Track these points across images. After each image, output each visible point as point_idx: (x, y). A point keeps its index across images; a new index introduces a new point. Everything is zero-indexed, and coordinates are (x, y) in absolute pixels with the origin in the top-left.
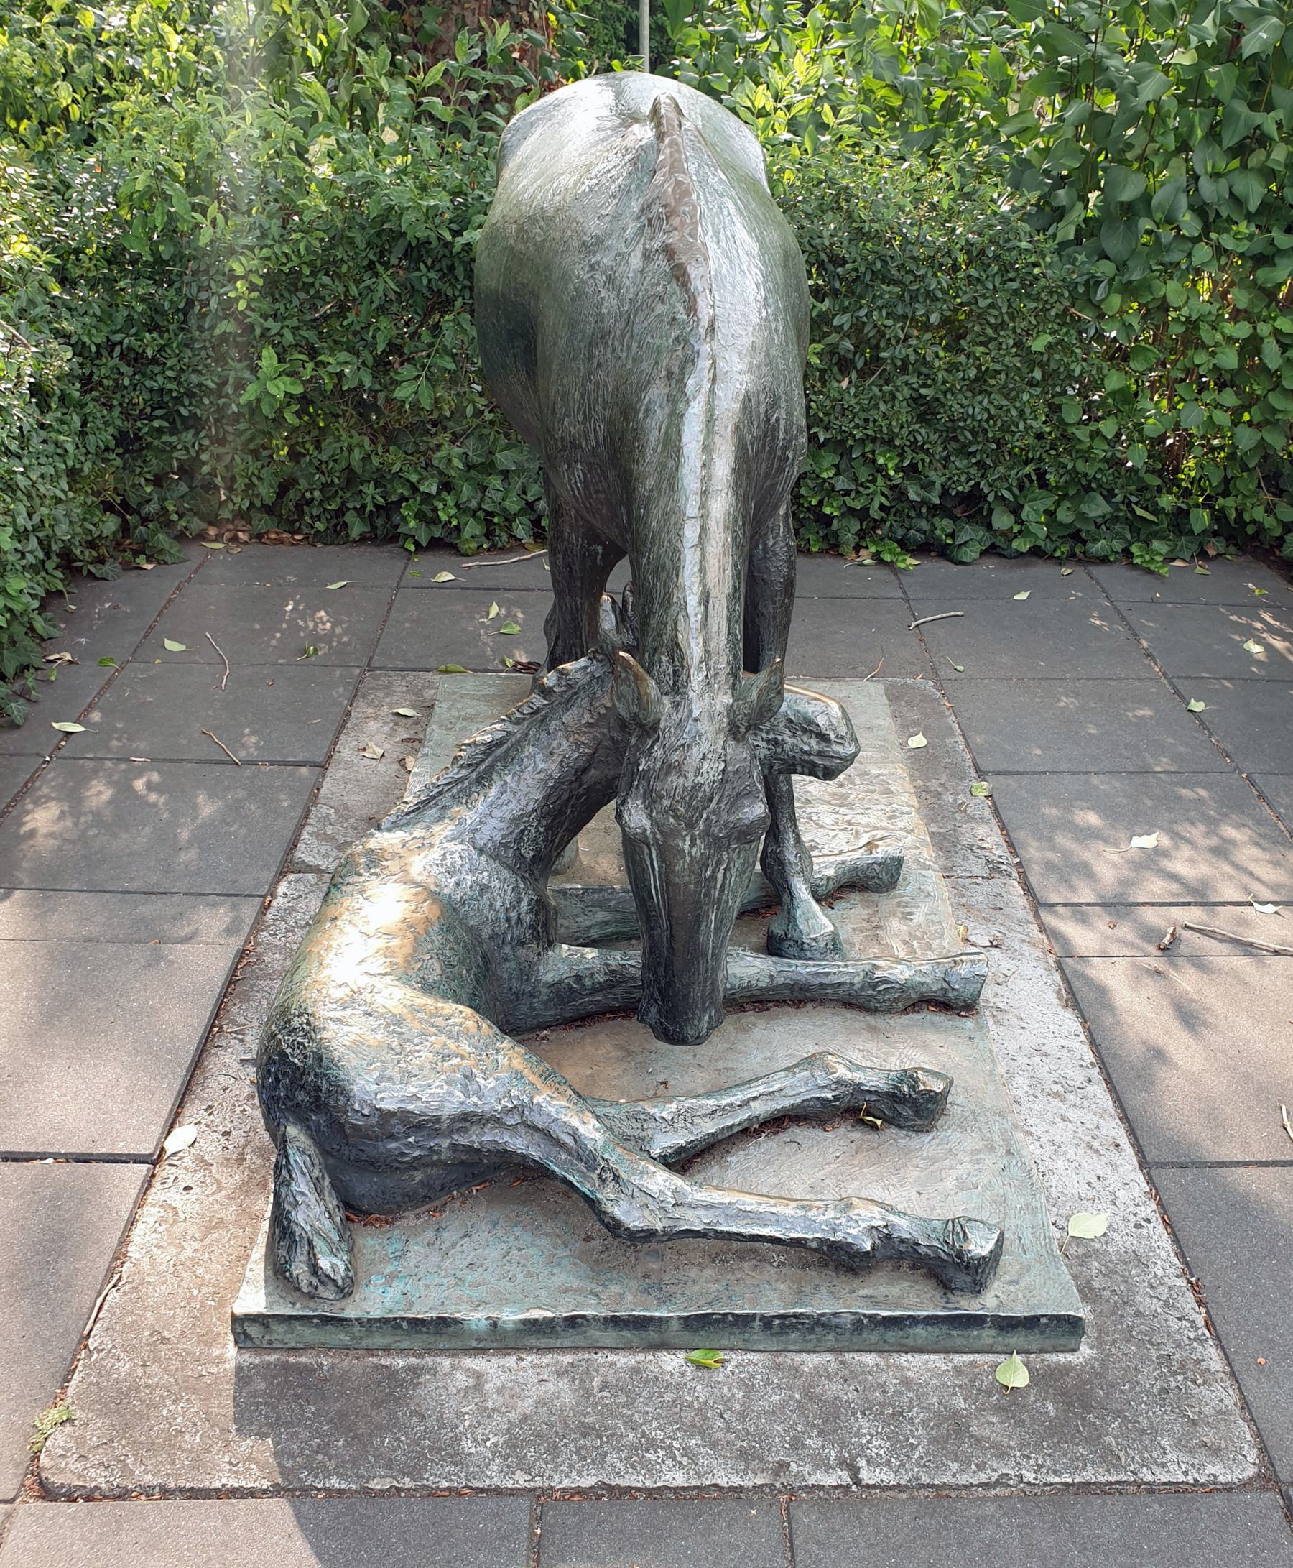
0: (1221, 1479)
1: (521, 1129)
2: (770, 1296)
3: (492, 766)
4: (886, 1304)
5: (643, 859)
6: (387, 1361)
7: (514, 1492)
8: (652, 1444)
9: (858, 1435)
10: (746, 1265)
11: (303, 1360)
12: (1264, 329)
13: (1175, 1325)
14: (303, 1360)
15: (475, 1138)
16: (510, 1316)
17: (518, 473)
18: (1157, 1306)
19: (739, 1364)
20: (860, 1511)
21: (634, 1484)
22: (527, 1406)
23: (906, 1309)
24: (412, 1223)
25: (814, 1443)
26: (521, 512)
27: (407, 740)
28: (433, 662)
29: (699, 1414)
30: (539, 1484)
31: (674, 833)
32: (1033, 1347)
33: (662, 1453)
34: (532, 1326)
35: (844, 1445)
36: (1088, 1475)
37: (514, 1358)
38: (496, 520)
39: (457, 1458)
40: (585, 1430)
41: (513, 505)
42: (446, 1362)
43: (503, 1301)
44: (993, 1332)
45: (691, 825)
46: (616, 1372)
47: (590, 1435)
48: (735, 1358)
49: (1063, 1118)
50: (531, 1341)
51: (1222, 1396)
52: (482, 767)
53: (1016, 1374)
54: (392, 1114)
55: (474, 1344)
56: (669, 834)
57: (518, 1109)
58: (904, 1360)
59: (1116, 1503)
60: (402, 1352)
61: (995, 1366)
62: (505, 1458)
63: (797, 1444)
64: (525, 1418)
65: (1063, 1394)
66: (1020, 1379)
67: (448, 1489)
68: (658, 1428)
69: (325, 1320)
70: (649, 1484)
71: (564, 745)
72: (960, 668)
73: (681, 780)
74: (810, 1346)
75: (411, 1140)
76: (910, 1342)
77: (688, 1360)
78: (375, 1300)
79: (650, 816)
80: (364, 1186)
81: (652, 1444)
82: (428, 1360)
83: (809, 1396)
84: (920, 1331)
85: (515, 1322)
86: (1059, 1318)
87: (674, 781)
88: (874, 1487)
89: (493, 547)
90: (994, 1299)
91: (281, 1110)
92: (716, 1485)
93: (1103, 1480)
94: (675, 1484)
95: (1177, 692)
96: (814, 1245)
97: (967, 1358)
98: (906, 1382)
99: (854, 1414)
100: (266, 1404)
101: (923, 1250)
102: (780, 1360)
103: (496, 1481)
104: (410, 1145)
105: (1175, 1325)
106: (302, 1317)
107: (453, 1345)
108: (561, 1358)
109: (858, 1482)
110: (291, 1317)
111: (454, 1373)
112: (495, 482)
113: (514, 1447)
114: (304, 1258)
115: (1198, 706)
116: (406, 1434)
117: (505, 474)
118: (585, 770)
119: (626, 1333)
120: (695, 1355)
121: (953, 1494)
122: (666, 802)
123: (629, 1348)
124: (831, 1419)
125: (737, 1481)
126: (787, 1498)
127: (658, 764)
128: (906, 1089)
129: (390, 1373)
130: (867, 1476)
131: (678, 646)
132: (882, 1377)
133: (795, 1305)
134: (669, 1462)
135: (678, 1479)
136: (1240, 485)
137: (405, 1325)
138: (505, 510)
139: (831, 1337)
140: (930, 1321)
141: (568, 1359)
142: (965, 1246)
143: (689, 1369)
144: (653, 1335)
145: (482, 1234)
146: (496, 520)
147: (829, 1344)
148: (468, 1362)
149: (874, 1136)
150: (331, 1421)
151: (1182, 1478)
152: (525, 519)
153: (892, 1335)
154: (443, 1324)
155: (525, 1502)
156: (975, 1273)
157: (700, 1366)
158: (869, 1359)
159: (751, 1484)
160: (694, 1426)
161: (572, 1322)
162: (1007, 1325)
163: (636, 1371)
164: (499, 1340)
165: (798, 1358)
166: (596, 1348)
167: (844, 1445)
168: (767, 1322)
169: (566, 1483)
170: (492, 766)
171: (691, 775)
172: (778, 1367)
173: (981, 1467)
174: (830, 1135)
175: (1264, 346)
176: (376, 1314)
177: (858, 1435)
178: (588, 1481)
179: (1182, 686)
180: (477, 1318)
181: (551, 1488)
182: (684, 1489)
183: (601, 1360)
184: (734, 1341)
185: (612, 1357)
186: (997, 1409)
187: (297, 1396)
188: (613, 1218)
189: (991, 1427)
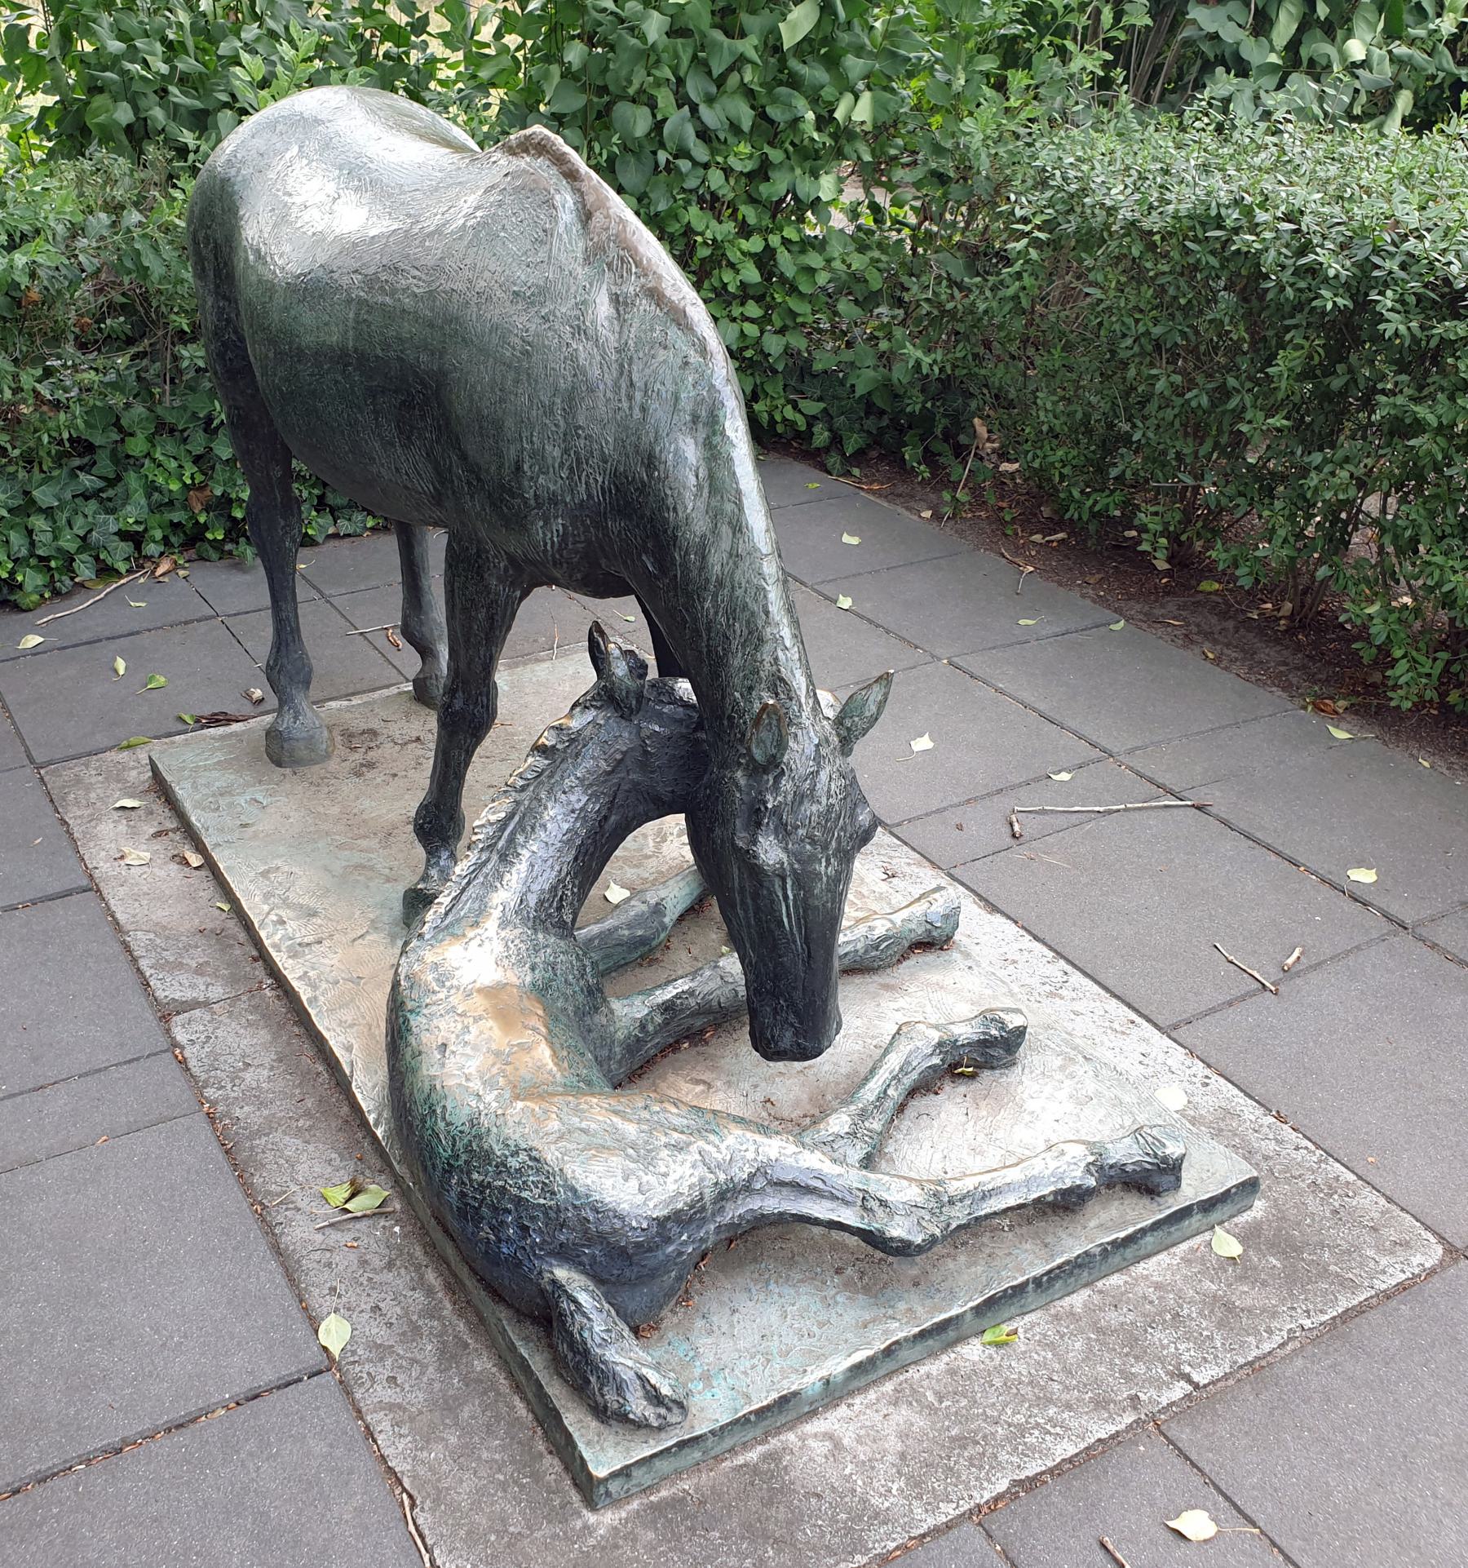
0: (1427, 1265)
1: (768, 1189)
2: (1028, 1261)
3: (511, 840)
4: (1125, 1224)
5: (772, 893)
6: (740, 1460)
7: (949, 1526)
8: (1022, 1430)
9: (1164, 1347)
10: (985, 1240)
11: (664, 1493)
12: (775, 240)
13: (1294, 1154)
14: (664, 1493)
15: (736, 1211)
16: (838, 1365)
17: (61, 508)
18: (1272, 1145)
19: (1028, 1326)
20: (1216, 1410)
21: (1039, 1470)
22: (893, 1444)
23: (1134, 1224)
24: (675, 1320)
25: (1139, 1369)
26: (80, 550)
27: (158, 834)
28: (101, 740)
29: (1039, 1386)
30: (967, 1507)
31: (813, 859)
32: (1225, 1217)
33: (1036, 1433)
34: (858, 1369)
35: (1162, 1360)
36: (1343, 1304)
37: (844, 1407)
38: (53, 564)
39: (880, 1517)
40: (961, 1442)
41: (68, 543)
42: (791, 1437)
43: (821, 1357)
44: (1199, 1216)
45: (825, 847)
46: (938, 1381)
47: (965, 1444)
48: (1019, 1323)
49: (1077, 1014)
50: (862, 1382)
51: (1369, 1202)
52: (501, 844)
53: (1227, 1244)
54: (667, 1218)
55: (806, 1409)
56: (807, 860)
57: (761, 1171)
58: (1141, 1268)
59: (1374, 1316)
60: (746, 1446)
61: (1209, 1244)
62: (919, 1497)
63: (1129, 1377)
64: (903, 1456)
65: (1273, 1245)
66: (1234, 1248)
67: (897, 1548)
68: (1014, 1414)
69: (682, 1445)
70: (1050, 1464)
71: (578, 799)
72: (632, 619)
73: (814, 808)
74: (1070, 1289)
75: (684, 1237)
76: (1142, 1252)
77: (984, 1345)
78: (712, 1408)
79: (786, 849)
80: (637, 1300)
81: (1022, 1430)
82: (774, 1443)
83: (1100, 1331)
84: (1149, 1239)
85: (844, 1373)
86: (1243, 1184)
87: (811, 809)
88: (1213, 1383)
89: (56, 593)
90: (1192, 1188)
91: (540, 1257)
92: (1099, 1440)
93: (1355, 1302)
94: (1069, 1454)
95: (827, 598)
96: (1051, 1198)
97: (1184, 1246)
98: (1158, 1286)
99: (1146, 1331)
100: (671, 1550)
101: (1129, 1168)
102: (1053, 1311)
103: (931, 1522)
104: (685, 1243)
105: (1294, 1154)
106: (661, 1452)
107: (789, 1418)
108: (883, 1389)
109: (1196, 1386)
110: (653, 1456)
111: (808, 1444)
112: (39, 523)
113: (917, 1485)
114: (640, 1393)
115: (845, 602)
116: (818, 1517)
117: (48, 512)
118: (606, 818)
119: (930, 1342)
120: (988, 1336)
121: (1263, 1363)
122: (801, 832)
123: (933, 1354)
124: (1133, 1342)
125: (1112, 1429)
126: (1156, 1424)
127: (790, 798)
128: (994, 1032)
129: (753, 1469)
130: (1201, 1377)
131: (782, 680)
132: (1139, 1291)
133: (1052, 1257)
134: (1048, 1438)
135: (1067, 1449)
136: (769, 389)
137: (753, 1418)
138: (59, 550)
139: (1085, 1274)
140: (1156, 1226)
141: (888, 1387)
142: (1168, 1152)
143: (992, 1350)
144: (951, 1334)
145: (746, 1306)
146: (53, 564)
147: (1084, 1281)
148: (810, 1428)
149: (975, 1086)
150: (743, 1538)
151: (1404, 1277)
152: (85, 557)
153: (1129, 1252)
154: (784, 1401)
155: (968, 1528)
156: (1171, 1169)
157: (999, 1345)
158: (1116, 1280)
159: (1123, 1426)
160: (1039, 1398)
161: (888, 1352)
162: (1208, 1206)
163: (952, 1372)
164: (833, 1393)
165: (1067, 1301)
166: (904, 1368)
167: (1162, 1360)
168: (1037, 1281)
169: (987, 1496)
170: (511, 840)
171: (824, 800)
172: (1057, 1317)
173: (1270, 1331)
174: (942, 1096)
175: (778, 256)
176: (725, 1419)
177: (1164, 1347)
178: (1002, 1486)
179: (827, 589)
180: (810, 1381)
181: (978, 1506)
182: (1077, 1455)
183: (917, 1376)
184: (1013, 1310)
185: (924, 1369)
186: (1241, 1278)
187: (693, 1530)
188: (902, 1241)
189: (1246, 1296)
